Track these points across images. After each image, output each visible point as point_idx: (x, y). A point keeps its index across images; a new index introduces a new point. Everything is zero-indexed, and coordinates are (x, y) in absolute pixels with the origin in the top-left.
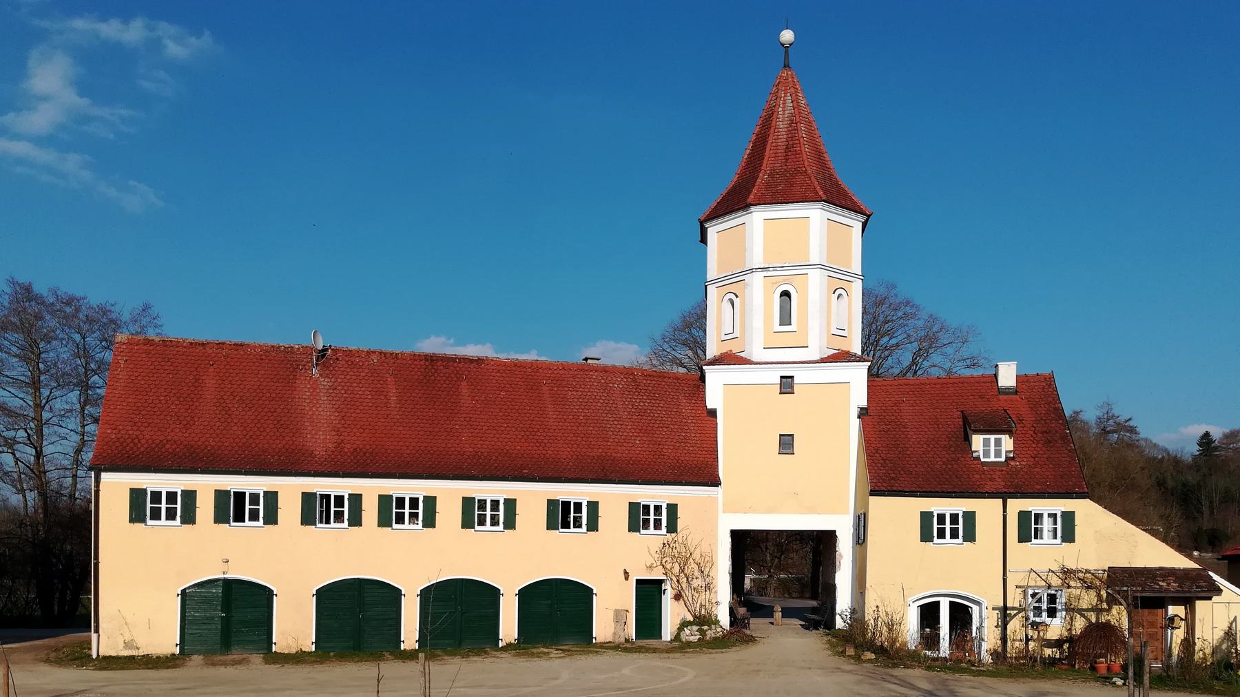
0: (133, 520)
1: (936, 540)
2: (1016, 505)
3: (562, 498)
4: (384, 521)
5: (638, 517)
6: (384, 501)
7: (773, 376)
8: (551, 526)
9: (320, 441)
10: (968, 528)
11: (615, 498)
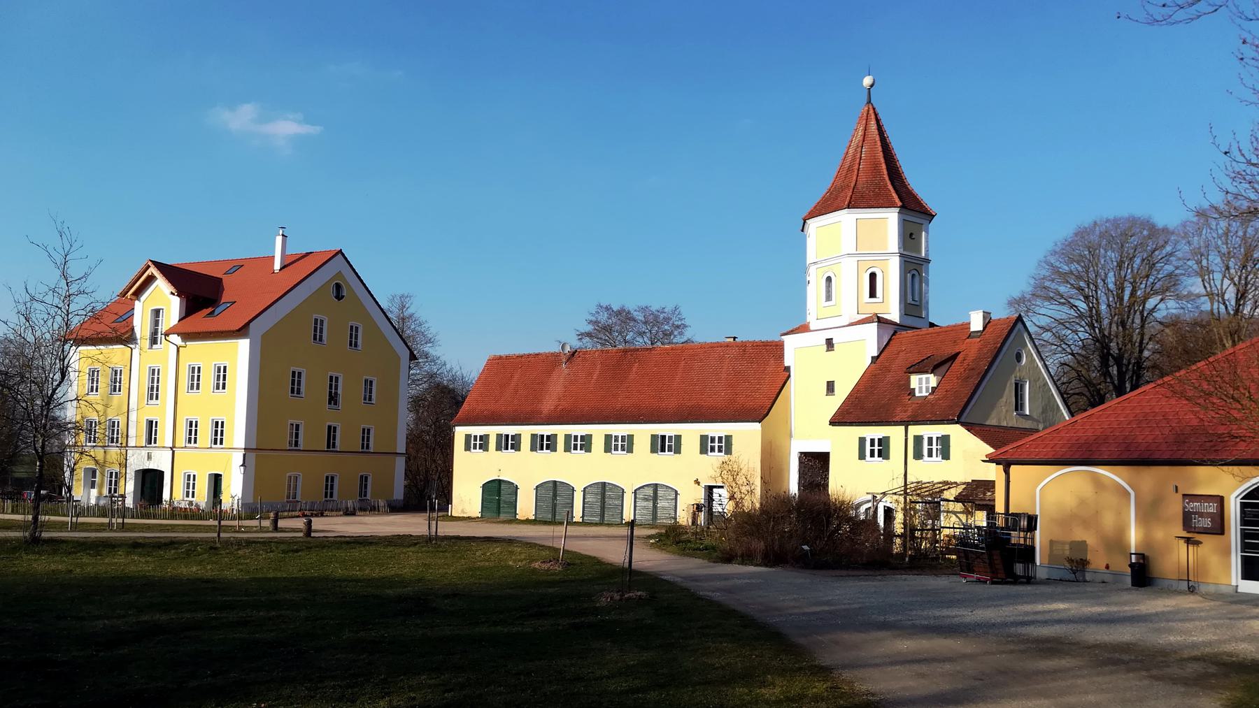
0: (701, 453)
1: (926, 457)
2: (914, 430)
3: (540, 433)
4: (567, 449)
5: (706, 445)
6: (568, 437)
7: (821, 338)
8: (653, 450)
9: (548, 405)
10: (628, 444)
11: (690, 432)
